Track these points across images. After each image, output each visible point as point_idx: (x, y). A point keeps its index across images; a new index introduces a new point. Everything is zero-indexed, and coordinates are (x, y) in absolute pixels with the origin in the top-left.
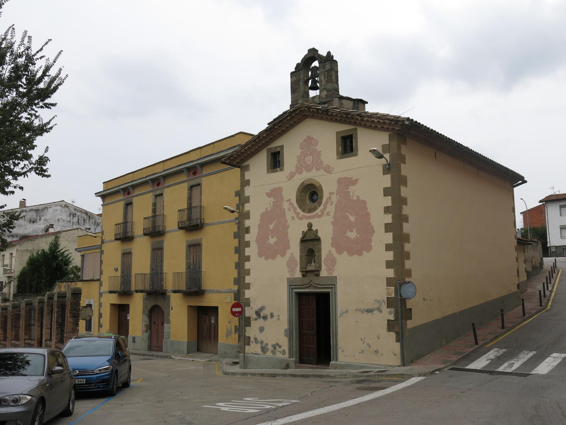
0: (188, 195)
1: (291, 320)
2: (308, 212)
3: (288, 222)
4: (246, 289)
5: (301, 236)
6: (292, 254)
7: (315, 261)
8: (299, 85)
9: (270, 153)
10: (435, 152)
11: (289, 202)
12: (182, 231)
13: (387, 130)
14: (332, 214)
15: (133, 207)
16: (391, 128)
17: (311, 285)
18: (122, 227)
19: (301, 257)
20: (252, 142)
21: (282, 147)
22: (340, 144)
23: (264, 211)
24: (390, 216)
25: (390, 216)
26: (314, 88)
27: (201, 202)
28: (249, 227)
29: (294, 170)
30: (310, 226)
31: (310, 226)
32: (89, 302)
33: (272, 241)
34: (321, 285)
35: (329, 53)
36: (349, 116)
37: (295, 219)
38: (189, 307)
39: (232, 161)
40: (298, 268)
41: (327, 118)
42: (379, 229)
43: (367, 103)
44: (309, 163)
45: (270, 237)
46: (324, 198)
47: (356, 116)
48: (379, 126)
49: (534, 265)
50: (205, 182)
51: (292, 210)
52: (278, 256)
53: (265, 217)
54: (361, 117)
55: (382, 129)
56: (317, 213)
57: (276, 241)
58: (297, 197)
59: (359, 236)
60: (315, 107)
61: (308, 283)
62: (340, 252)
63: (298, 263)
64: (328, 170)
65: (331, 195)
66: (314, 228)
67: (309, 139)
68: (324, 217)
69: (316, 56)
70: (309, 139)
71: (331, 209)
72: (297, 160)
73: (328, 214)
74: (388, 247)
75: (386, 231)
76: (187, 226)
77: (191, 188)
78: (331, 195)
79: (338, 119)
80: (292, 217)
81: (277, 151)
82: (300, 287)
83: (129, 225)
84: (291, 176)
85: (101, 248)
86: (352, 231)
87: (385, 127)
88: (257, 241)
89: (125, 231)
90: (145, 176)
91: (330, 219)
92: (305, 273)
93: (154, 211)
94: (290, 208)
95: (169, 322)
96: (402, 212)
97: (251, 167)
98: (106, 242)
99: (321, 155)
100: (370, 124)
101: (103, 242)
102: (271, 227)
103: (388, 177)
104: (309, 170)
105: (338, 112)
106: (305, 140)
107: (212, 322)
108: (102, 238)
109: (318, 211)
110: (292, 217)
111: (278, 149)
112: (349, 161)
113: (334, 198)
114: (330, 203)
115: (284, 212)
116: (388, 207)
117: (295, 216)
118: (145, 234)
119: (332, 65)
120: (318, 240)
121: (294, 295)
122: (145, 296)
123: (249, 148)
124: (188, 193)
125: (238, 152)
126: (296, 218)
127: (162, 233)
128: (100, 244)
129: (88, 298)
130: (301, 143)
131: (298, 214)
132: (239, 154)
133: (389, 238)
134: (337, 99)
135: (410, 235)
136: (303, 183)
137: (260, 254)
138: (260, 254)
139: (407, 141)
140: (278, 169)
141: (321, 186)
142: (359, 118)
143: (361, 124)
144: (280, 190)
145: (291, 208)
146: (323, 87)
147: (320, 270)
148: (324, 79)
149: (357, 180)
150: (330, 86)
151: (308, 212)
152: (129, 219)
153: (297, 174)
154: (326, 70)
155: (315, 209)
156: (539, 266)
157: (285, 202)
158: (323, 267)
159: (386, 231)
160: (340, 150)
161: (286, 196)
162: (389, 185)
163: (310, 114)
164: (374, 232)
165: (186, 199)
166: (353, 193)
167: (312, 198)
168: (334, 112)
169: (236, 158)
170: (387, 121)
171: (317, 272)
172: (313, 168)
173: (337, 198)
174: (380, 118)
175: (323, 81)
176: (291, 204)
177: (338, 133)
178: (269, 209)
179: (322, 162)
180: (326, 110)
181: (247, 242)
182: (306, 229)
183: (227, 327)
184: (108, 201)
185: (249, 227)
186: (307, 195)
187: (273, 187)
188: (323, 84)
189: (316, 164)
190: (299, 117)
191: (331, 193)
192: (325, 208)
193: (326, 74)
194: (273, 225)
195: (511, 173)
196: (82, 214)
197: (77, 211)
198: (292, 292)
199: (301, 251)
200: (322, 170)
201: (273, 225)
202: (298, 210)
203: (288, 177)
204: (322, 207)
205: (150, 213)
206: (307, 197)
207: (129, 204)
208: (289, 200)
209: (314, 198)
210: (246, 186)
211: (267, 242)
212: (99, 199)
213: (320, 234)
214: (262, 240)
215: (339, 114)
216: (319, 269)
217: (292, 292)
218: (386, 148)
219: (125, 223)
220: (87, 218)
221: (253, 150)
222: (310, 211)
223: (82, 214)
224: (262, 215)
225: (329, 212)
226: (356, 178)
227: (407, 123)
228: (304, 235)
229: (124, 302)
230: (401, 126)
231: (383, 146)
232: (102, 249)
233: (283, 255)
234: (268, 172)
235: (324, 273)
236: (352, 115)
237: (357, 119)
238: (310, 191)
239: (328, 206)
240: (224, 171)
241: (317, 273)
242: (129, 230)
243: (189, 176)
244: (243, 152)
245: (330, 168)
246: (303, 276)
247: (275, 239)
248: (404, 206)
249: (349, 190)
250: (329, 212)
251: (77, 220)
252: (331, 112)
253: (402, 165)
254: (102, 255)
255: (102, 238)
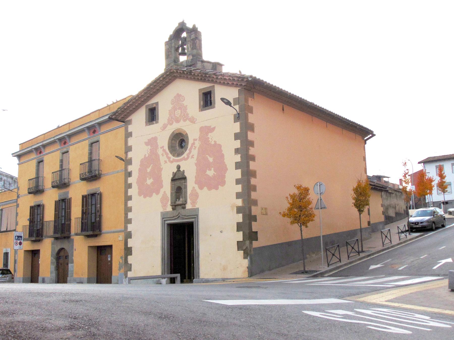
0: (89, 151)
1: (163, 246)
2: (177, 156)
3: (161, 166)
4: (129, 223)
5: (172, 176)
6: (165, 192)
7: (182, 197)
8: (171, 52)
9: (148, 109)
10: (283, 105)
11: (162, 149)
12: (84, 182)
13: (237, 86)
14: (195, 157)
15: (44, 164)
16: (239, 84)
17: (179, 216)
18: (34, 182)
19: (171, 193)
20: (133, 100)
21: (157, 103)
22: (201, 99)
23: (143, 157)
24: (239, 155)
25: (239, 155)
26: (183, 54)
27: (99, 156)
28: (132, 171)
29: (166, 122)
30: (179, 167)
31: (179, 167)
32: (6, 250)
33: (149, 181)
34: (187, 216)
35: (194, 26)
36: (207, 76)
37: (167, 163)
38: (90, 247)
39: (118, 117)
40: (169, 203)
41: (191, 78)
42: (231, 166)
43: (223, 65)
44: (178, 116)
45: (148, 179)
46: (189, 144)
47: (213, 75)
48: (230, 83)
49: (397, 211)
50: (102, 138)
51: (165, 156)
52: (154, 194)
53: (145, 163)
54: (216, 75)
55: (232, 85)
56: (184, 157)
57: (152, 182)
58: (169, 144)
59: (216, 173)
60: (181, 69)
61: (177, 215)
62: (201, 188)
63: (169, 199)
64: (193, 121)
65: (195, 142)
66: (181, 169)
67: (179, 96)
68: (189, 159)
69: (184, 27)
70: (179, 96)
71: (195, 152)
72: (169, 114)
73: (192, 157)
74: (238, 182)
75: (236, 168)
76: (88, 177)
77: (91, 144)
78: (195, 142)
79: (200, 78)
80: (165, 161)
81: (153, 107)
82: (171, 219)
83: (41, 179)
84: (164, 127)
85: (17, 202)
86: (210, 170)
87: (235, 83)
88: (137, 183)
89: (37, 186)
90: (53, 137)
91: (194, 160)
92: (174, 207)
93: (61, 166)
94: (163, 153)
95: (72, 262)
96: (249, 152)
97: (133, 121)
98: (21, 196)
99: (187, 109)
100: (223, 81)
101: (18, 197)
102: (149, 170)
103: (238, 124)
104: (178, 121)
105: (199, 73)
106: (175, 97)
107: (109, 260)
108: (18, 193)
109: (185, 155)
110: (165, 161)
111: (154, 106)
112: (209, 112)
113: (197, 144)
114: (194, 147)
115: (159, 157)
116: (238, 149)
117: (167, 160)
118: (53, 187)
119: (196, 35)
120: (185, 178)
121: (166, 225)
122: (52, 241)
123: (131, 105)
124: (89, 149)
125: (122, 109)
126: (168, 162)
127: (68, 184)
128: (16, 198)
129: (5, 247)
130: (172, 100)
131: (169, 158)
132: (122, 110)
133: (238, 174)
134: (200, 62)
135: (257, 171)
136: (173, 132)
137: (140, 194)
138: (140, 194)
139: (254, 95)
140: (154, 122)
141: (187, 134)
142: (215, 77)
143: (217, 81)
144: (155, 139)
145: (164, 154)
146: (189, 53)
147: (186, 204)
148: (190, 47)
149: (214, 128)
150: (195, 52)
151: (177, 156)
152: (40, 175)
153: (169, 125)
154: (192, 38)
155: (183, 153)
156: (403, 213)
157: (159, 149)
158: (189, 201)
159: (236, 168)
160: (202, 104)
161: (160, 145)
162: (238, 130)
163: (178, 75)
164: (227, 169)
165: (87, 154)
166: (211, 139)
167: (181, 145)
168: (196, 72)
169: (120, 114)
170: (235, 79)
171: (184, 206)
172: (181, 120)
173: (199, 143)
174: (230, 76)
175: (189, 48)
176: (164, 150)
177: (200, 90)
178: (147, 156)
179: (188, 114)
180: (190, 71)
181: (130, 184)
182: (175, 170)
183: (119, 262)
184: (24, 159)
185: (132, 171)
186: (177, 142)
187: (150, 137)
188: (190, 50)
189: (184, 116)
190: (170, 78)
191: (195, 140)
192: (190, 152)
193: (192, 42)
194: (150, 168)
195: (358, 127)
196: (8, 179)
197: (3, 175)
198: (164, 224)
199: (172, 189)
200: (188, 121)
201: (150, 168)
202: (170, 155)
203: (162, 128)
204: (188, 151)
205: (57, 168)
206: (177, 144)
207: (40, 162)
208: (163, 147)
209: (183, 145)
210: (129, 137)
211: (145, 183)
212: (16, 158)
213: (186, 174)
214: (141, 181)
215: (200, 74)
216: (185, 203)
217: (164, 224)
218: (237, 101)
219: (37, 178)
220: (12, 182)
221: (134, 107)
222: (179, 155)
223: (8, 179)
224: (142, 161)
225: (193, 155)
226: (214, 126)
227: (250, 79)
228: (174, 175)
229: (35, 247)
230: (246, 82)
231: (234, 99)
232: (18, 203)
233: (158, 193)
234: (146, 125)
235: (189, 206)
236: (210, 75)
237: (213, 77)
238: (180, 139)
239: (193, 150)
240: (116, 129)
241: (183, 206)
242: (40, 184)
243: (90, 134)
244: (126, 109)
245: (194, 119)
246: (173, 209)
247: (151, 180)
248: (250, 148)
249: (208, 136)
250: (193, 155)
251: (3, 184)
252: (193, 73)
253: (250, 115)
254: (18, 208)
255: (18, 193)
